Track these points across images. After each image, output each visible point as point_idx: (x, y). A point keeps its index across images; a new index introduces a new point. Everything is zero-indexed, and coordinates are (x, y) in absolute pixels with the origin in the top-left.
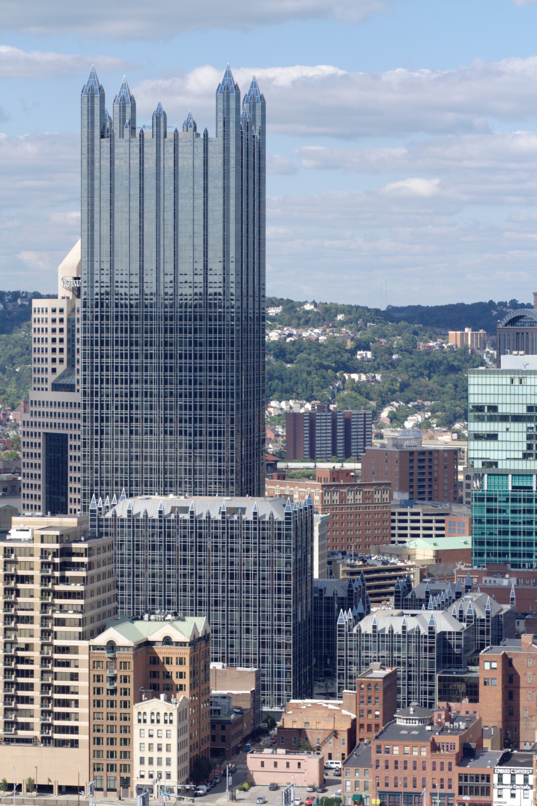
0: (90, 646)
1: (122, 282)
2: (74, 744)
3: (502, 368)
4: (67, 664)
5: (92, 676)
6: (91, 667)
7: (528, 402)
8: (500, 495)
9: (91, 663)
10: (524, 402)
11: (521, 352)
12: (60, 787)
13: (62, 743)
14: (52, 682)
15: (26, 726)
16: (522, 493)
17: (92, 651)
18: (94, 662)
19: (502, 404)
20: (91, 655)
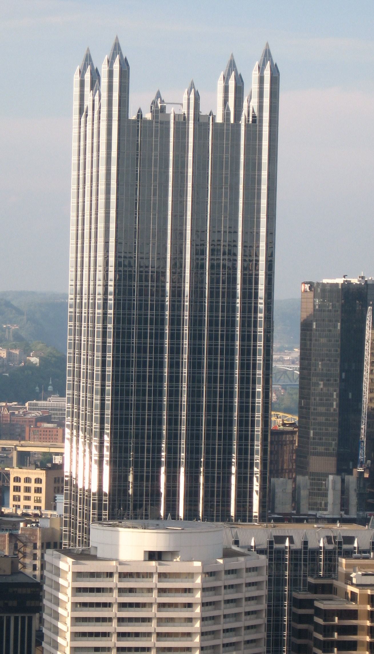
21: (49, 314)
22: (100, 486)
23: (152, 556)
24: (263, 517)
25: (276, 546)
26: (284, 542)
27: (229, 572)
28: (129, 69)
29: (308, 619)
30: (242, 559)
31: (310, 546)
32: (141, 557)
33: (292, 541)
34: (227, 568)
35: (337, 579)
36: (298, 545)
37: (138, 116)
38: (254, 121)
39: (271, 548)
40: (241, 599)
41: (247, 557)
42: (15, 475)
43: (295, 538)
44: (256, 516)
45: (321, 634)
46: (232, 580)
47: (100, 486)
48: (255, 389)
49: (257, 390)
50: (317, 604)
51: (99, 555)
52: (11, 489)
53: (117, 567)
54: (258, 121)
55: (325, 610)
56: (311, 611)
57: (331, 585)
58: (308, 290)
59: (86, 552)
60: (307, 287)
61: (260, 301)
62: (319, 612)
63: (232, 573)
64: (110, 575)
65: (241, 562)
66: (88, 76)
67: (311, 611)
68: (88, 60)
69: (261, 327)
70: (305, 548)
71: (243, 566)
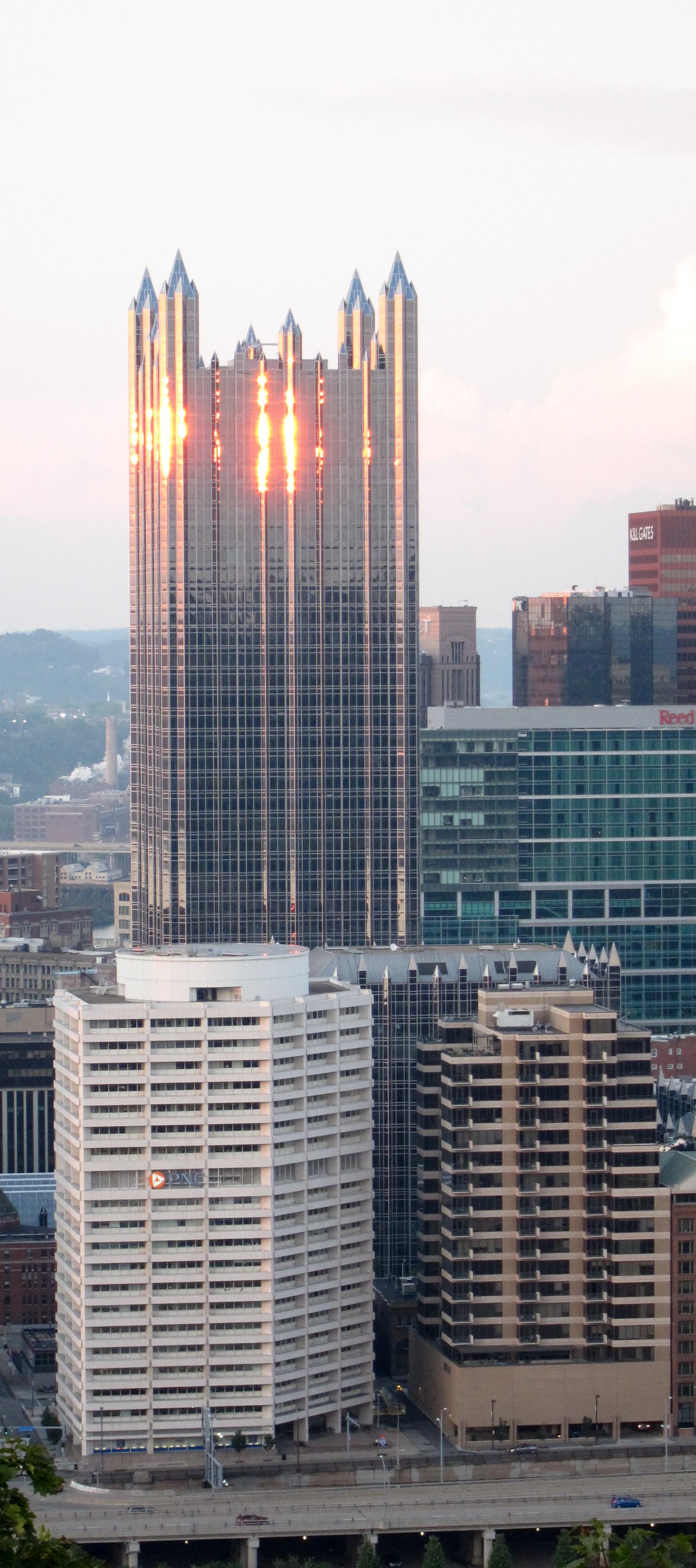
0: (672, 1196)
1: (199, 581)
2: (648, 1354)
3: (429, 728)
4: (632, 1226)
5: (676, 1244)
6: (675, 1230)
7: (462, 780)
8: (482, 924)
9: (675, 1223)
10: (456, 780)
11: (460, 703)
12: (624, 1425)
13: (629, 1354)
14: (609, 1257)
15: (557, 1331)
16: (441, 921)
17: (675, 1204)
18: (679, 1220)
19: (447, 783)
20: (675, 1211)
21: (44, 652)
22: (175, 900)
23: (204, 994)
24: (412, 939)
25: (421, 979)
26: (432, 972)
27: (315, 1015)
28: (197, 297)
29: (432, 1079)
30: (333, 996)
31: (470, 978)
32: (185, 995)
33: (444, 970)
34: (311, 1009)
35: (477, 1021)
36: (452, 977)
37: (213, 363)
38: (382, 366)
39: (413, 981)
40: (334, 1052)
41: (341, 994)
42: (122, 891)
43: (450, 967)
44: (402, 937)
45: (449, 1099)
46: (318, 1026)
47: (175, 900)
48: (395, 752)
49: (399, 754)
50: (445, 1057)
51: (128, 996)
52: (117, 910)
53: (148, 1012)
54: (387, 366)
55: (454, 1066)
56: (437, 1069)
57: (470, 1031)
58: (520, 609)
59: (112, 993)
60: (519, 603)
61: (399, 625)
62: (449, 1070)
63: (320, 1016)
64: (139, 1023)
65: (331, 1001)
66: (146, 312)
67: (437, 1069)
68: (357, 285)
69: (400, 663)
70: (463, 980)
71: (336, 1006)
